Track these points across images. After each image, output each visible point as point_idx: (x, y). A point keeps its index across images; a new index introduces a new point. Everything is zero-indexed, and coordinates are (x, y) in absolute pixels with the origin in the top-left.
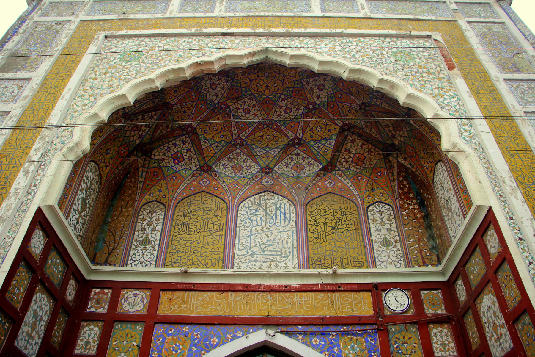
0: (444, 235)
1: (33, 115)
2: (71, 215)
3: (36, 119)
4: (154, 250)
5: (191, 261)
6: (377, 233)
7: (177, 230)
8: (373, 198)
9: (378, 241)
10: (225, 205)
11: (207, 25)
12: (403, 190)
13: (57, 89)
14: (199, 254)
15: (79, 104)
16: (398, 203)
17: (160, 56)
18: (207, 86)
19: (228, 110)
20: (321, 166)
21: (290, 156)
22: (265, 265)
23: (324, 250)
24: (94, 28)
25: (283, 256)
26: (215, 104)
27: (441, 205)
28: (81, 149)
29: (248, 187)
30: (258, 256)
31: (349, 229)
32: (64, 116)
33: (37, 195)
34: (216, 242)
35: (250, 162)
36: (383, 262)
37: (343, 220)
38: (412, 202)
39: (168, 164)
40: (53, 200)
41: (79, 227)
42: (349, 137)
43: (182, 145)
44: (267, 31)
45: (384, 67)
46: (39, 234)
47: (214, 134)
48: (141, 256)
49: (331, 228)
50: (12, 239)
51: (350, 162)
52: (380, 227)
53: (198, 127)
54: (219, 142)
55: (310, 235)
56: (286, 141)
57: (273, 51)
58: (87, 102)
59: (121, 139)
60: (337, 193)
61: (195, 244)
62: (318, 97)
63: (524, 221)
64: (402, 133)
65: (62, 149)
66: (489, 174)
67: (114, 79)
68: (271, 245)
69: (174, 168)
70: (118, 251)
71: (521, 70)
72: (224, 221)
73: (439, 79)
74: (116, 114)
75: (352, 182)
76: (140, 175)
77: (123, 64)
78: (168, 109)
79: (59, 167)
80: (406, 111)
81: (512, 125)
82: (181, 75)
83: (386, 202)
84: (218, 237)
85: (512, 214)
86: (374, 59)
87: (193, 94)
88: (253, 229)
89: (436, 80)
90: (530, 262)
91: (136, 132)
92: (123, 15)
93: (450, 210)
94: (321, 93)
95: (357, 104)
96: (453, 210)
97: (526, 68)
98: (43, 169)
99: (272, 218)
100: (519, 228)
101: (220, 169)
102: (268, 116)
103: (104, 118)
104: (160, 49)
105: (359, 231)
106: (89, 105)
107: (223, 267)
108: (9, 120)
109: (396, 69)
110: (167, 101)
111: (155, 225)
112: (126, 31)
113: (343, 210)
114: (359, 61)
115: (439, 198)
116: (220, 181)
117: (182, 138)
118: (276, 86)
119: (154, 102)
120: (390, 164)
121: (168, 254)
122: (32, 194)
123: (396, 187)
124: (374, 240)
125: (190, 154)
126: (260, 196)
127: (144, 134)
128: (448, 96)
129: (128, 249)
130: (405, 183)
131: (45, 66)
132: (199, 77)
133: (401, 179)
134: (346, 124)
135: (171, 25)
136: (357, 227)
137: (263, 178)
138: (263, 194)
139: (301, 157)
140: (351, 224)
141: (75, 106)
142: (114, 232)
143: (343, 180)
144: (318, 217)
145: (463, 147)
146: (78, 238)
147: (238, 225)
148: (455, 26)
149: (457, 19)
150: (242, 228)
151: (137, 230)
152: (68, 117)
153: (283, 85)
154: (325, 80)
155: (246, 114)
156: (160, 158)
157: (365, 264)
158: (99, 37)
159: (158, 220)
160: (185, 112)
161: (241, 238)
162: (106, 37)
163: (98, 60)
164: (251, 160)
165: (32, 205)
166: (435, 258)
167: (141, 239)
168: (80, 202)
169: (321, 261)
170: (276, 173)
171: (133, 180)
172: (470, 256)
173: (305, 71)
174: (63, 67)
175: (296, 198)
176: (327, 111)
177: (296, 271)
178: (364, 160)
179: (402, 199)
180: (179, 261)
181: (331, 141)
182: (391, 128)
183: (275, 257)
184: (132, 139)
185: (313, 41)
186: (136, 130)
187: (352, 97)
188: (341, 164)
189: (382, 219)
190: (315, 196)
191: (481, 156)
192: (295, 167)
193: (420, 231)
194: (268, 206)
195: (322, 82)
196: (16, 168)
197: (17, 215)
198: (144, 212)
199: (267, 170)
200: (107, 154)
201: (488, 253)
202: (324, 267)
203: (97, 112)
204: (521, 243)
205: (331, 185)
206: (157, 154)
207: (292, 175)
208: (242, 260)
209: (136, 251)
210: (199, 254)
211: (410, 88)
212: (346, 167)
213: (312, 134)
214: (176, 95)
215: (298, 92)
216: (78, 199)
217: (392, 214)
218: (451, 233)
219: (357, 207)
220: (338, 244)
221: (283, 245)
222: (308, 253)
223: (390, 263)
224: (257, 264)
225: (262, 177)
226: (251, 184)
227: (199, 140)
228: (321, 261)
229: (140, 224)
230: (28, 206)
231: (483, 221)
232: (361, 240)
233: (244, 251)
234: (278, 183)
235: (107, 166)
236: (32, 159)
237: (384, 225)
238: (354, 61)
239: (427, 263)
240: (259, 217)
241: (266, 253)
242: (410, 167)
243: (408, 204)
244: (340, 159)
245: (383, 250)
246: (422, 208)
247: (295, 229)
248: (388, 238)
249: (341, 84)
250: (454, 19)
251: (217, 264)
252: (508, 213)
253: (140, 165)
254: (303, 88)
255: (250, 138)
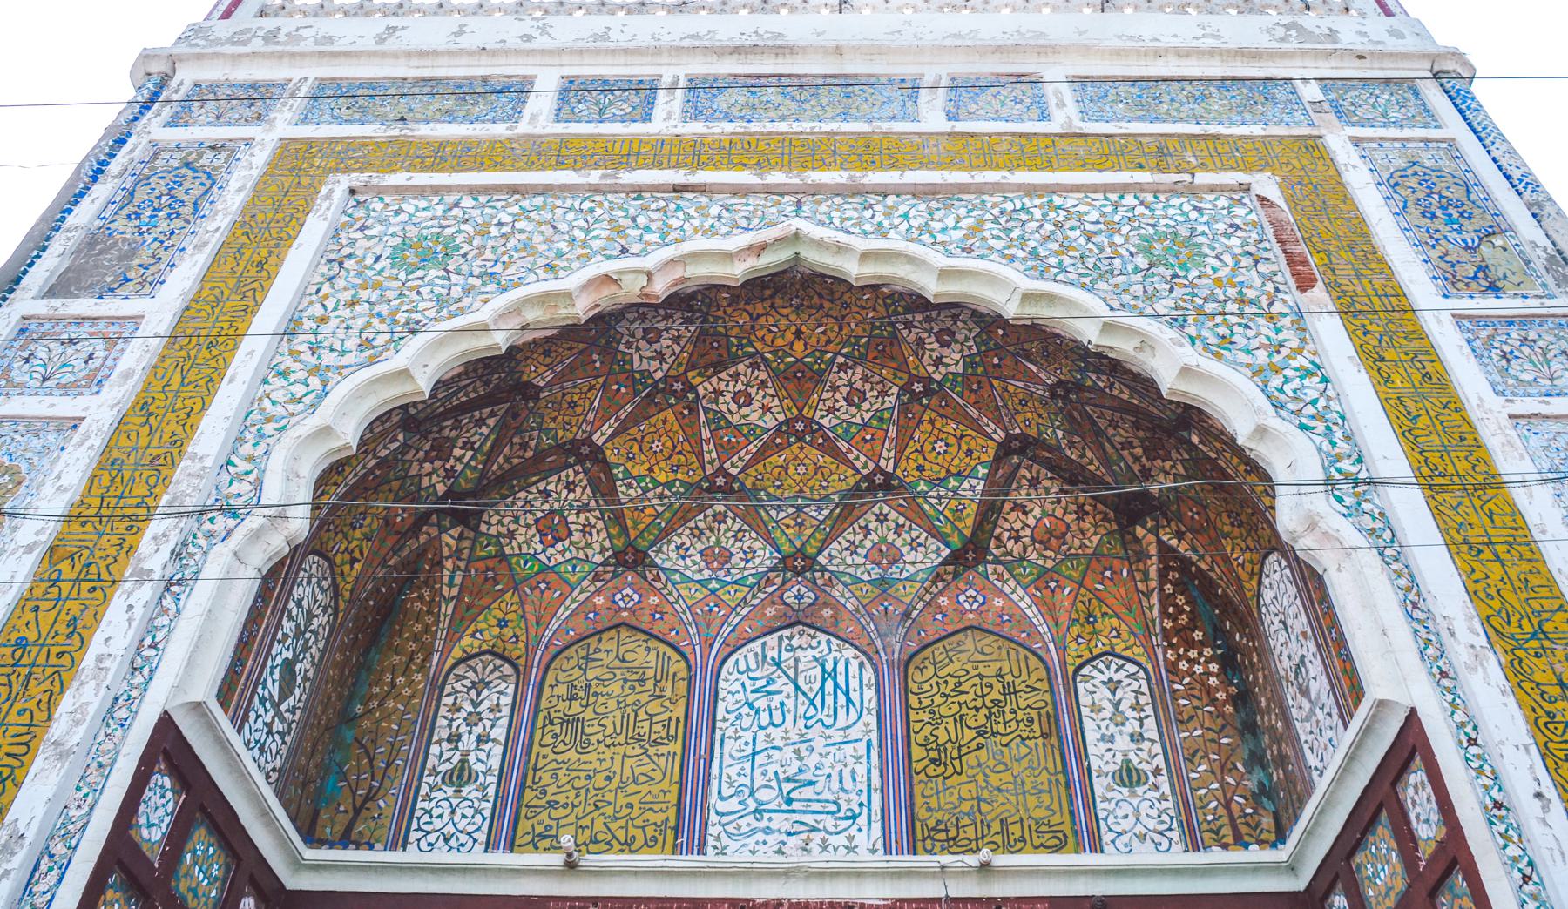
0: (1293, 760)
1: (146, 429)
2: (252, 715)
3: (154, 443)
4: (484, 798)
5: (587, 832)
6: (1103, 746)
7: (548, 740)
8: (1092, 644)
9: (1105, 769)
10: (683, 664)
11: (633, 159)
12: (1175, 620)
13: (215, 352)
14: (609, 811)
15: (278, 396)
16: (1160, 657)
17: (504, 254)
18: (633, 336)
19: (691, 396)
20: (948, 551)
21: (862, 522)
22: (793, 841)
23: (954, 799)
24: (317, 162)
25: (841, 814)
26: (657, 382)
27: (1282, 673)
28: (286, 533)
29: (747, 610)
30: (773, 815)
31: (1025, 735)
32: (235, 434)
33: (157, 675)
34: (658, 775)
35: (751, 541)
36: (1119, 834)
37: (1007, 709)
38: (1201, 654)
39: (524, 547)
40: (204, 689)
41: (274, 746)
42: (1023, 471)
43: (565, 492)
44: (796, 181)
45: (1116, 286)
46: (162, 787)
47: (653, 461)
48: (446, 818)
49: (973, 733)
50: (86, 808)
51: (1027, 540)
52: (1113, 728)
53: (609, 445)
54: (669, 485)
55: (917, 752)
56: (852, 481)
57: (812, 240)
58: (299, 390)
59: (396, 485)
60: (991, 628)
61: (599, 781)
62: (938, 362)
63: (1508, 751)
64: (1168, 464)
65: (229, 533)
66: (1410, 608)
67: (375, 321)
68: (811, 783)
69: (542, 557)
70: (381, 803)
71: (1500, 284)
72: (680, 711)
73: (1271, 317)
74: (383, 423)
75: (1032, 596)
76: (446, 579)
77: (402, 276)
78: (526, 399)
79: (218, 598)
80: (1179, 411)
81: (1476, 455)
82: (563, 312)
83: (1128, 653)
84: (663, 759)
85: (1475, 728)
86: (1090, 262)
87: (595, 357)
88: (761, 735)
89: (1261, 321)
90: (1524, 876)
91: (438, 463)
92: (400, 125)
93: (1305, 692)
94: (945, 351)
95: (1043, 383)
96: (1313, 695)
97: (1516, 279)
98: (177, 597)
99: (812, 703)
100: (1493, 772)
101: (669, 559)
102: (800, 412)
103: (349, 439)
104: (505, 229)
105: (1054, 740)
106: (307, 400)
107: (676, 849)
108: (81, 444)
109: (1150, 289)
110: (525, 378)
111: (488, 724)
112: (408, 175)
113: (1009, 678)
114: (1047, 270)
115: (1276, 653)
116: (670, 593)
117: (563, 474)
118: (824, 333)
119: (487, 383)
120: (1137, 548)
121: (524, 810)
122: (146, 671)
123: (1156, 612)
124: (1094, 767)
125: (587, 519)
126: (781, 638)
127: (459, 467)
128: (1296, 369)
129: (411, 795)
130: (1180, 600)
131: (182, 279)
132: (611, 314)
133: (1169, 588)
134: (1016, 437)
135: (534, 158)
136: (1046, 730)
137: (788, 586)
138: (787, 632)
139: (893, 525)
140: (1031, 720)
141: (267, 403)
142: (370, 746)
143: (1007, 589)
144: (938, 700)
145: (1336, 526)
146: (268, 777)
147: (718, 724)
148: (1316, 153)
149: (1323, 132)
150: (729, 732)
151: (435, 738)
152: (248, 436)
153: (841, 329)
154: (955, 318)
155: (740, 407)
156: (503, 530)
157: (1071, 840)
158: (331, 191)
159: (496, 708)
160: (572, 405)
161: (727, 761)
162: (352, 192)
163: (330, 261)
164: (754, 535)
165: (143, 705)
166: (1267, 821)
167: (447, 766)
168: (276, 676)
169: (947, 831)
170: (824, 570)
171: (426, 593)
172: (1364, 834)
173: (901, 294)
174: (232, 282)
175: (878, 643)
176: (960, 401)
177: (879, 860)
178: (1064, 534)
179: (1171, 646)
180: (553, 832)
181: (974, 482)
182: (1139, 451)
183: (819, 817)
184: (425, 482)
185: (923, 206)
186: (438, 458)
187: (1031, 366)
188: (1000, 543)
189: (1117, 705)
190: (932, 639)
191: (1388, 552)
192: (875, 554)
193: (1225, 741)
194: (801, 668)
195: (949, 324)
196: (99, 594)
197: (101, 737)
198: (458, 686)
199: (799, 563)
200: (355, 528)
201: (1413, 838)
202: (954, 849)
203: (329, 421)
204: (1501, 819)
205: (976, 605)
206: (494, 520)
207: (866, 577)
208: (730, 828)
209: (433, 804)
210: (609, 811)
211: (1188, 348)
212: (1015, 553)
213: (921, 461)
214: (548, 360)
215: (882, 349)
216: (273, 668)
217: (1145, 689)
218: (1312, 760)
219: (1048, 669)
220: (994, 780)
221: (841, 782)
222: (911, 806)
223: (1142, 838)
224: (771, 839)
225: (784, 582)
226: (755, 602)
227: (612, 479)
228: (947, 831)
229: (445, 722)
230: (134, 708)
231: (1394, 744)
232: (1059, 768)
233: (735, 800)
234: (828, 599)
235: (353, 561)
236: (146, 566)
237: (1123, 724)
238: (1034, 268)
239: (1247, 838)
240: (777, 699)
241: (796, 805)
242: (1195, 558)
243: (1189, 661)
244: (998, 530)
245: (1120, 797)
246: (1230, 673)
247: (874, 736)
248: (1135, 761)
249: (1001, 332)
250: (1315, 133)
251: (660, 839)
252: (1462, 725)
253: (446, 552)
254: (894, 337)
255: (752, 471)
